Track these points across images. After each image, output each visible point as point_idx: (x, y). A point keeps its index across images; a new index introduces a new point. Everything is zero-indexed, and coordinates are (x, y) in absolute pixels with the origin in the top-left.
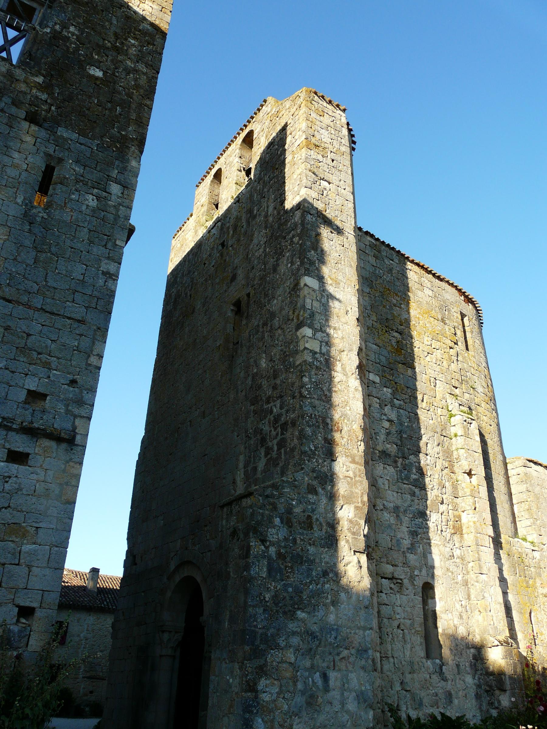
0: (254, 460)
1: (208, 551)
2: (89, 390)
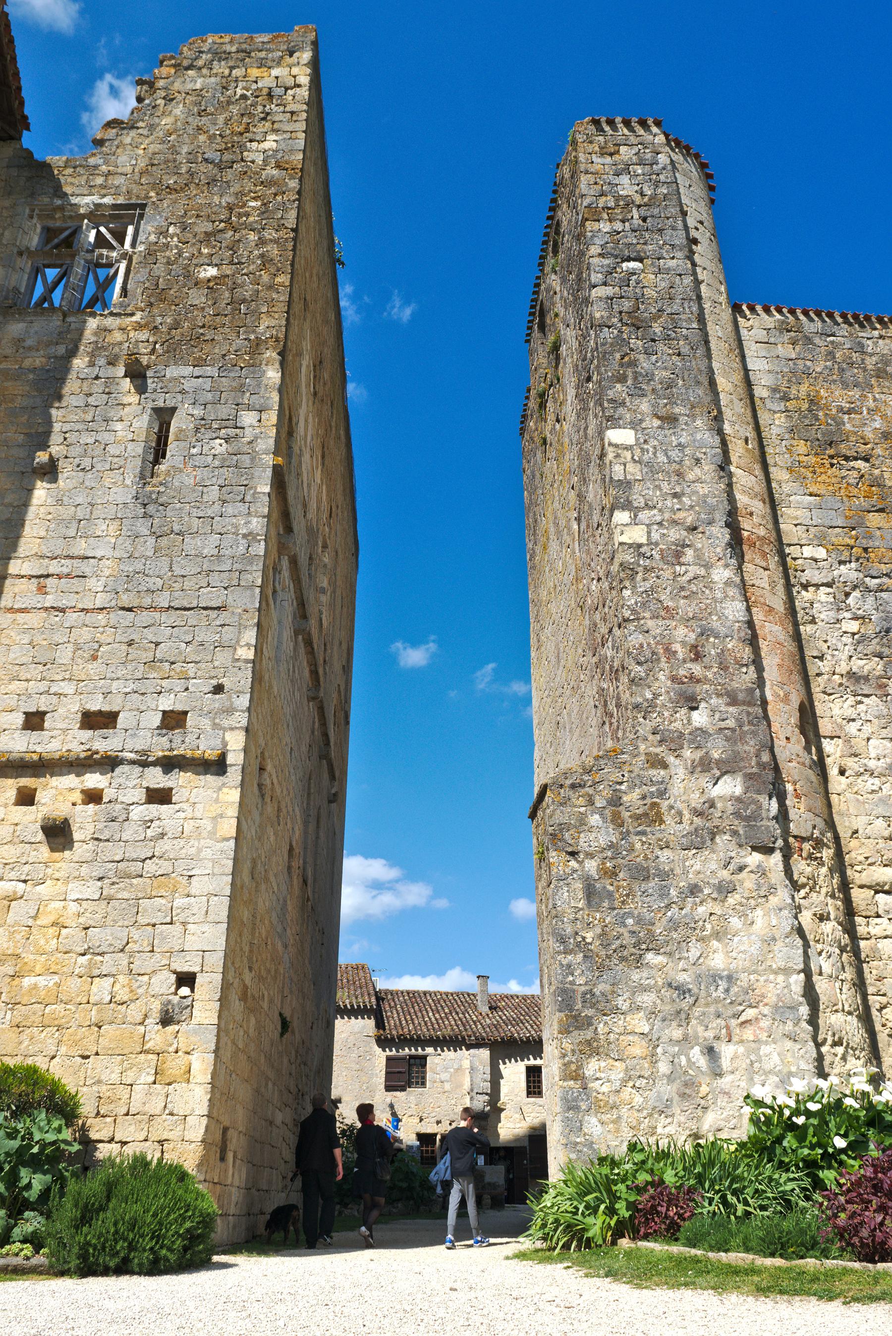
2: (240, 692)
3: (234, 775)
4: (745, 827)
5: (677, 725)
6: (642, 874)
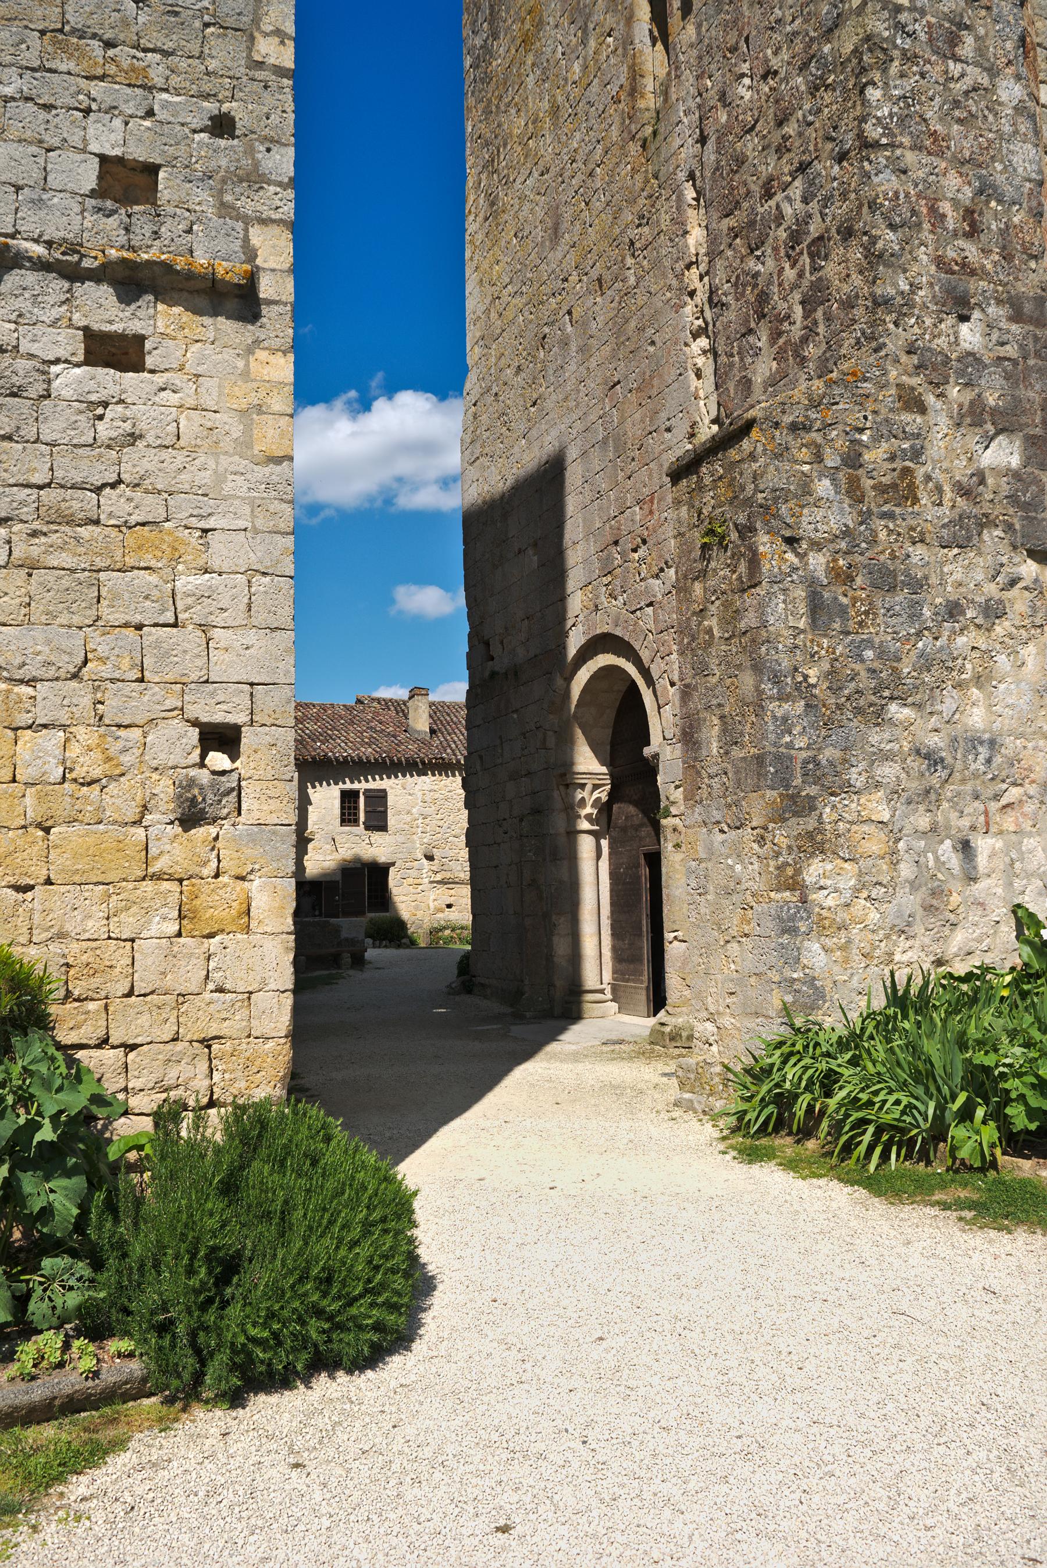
0: (742, 360)
1: (648, 606)
2: (272, 141)
3: (278, 323)
4: (1023, 518)
5: (941, 342)
6: (886, 580)
